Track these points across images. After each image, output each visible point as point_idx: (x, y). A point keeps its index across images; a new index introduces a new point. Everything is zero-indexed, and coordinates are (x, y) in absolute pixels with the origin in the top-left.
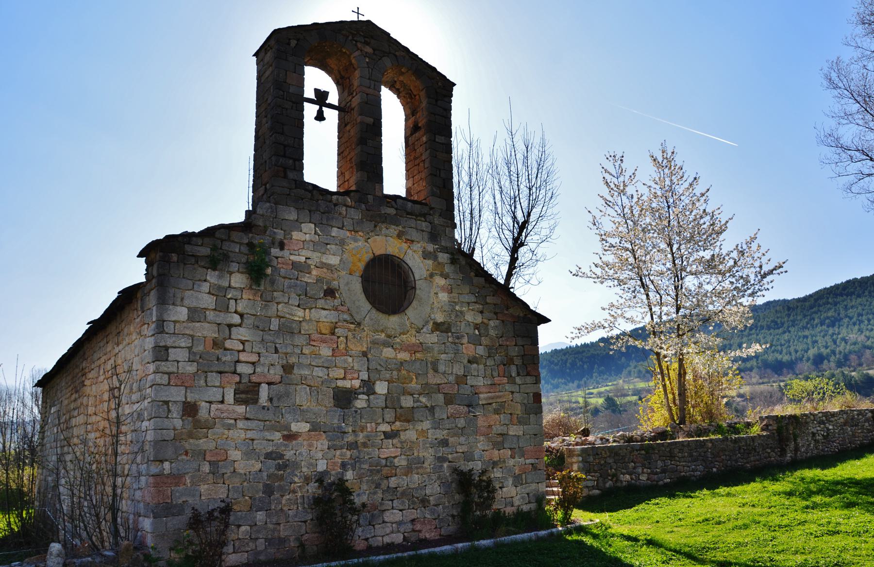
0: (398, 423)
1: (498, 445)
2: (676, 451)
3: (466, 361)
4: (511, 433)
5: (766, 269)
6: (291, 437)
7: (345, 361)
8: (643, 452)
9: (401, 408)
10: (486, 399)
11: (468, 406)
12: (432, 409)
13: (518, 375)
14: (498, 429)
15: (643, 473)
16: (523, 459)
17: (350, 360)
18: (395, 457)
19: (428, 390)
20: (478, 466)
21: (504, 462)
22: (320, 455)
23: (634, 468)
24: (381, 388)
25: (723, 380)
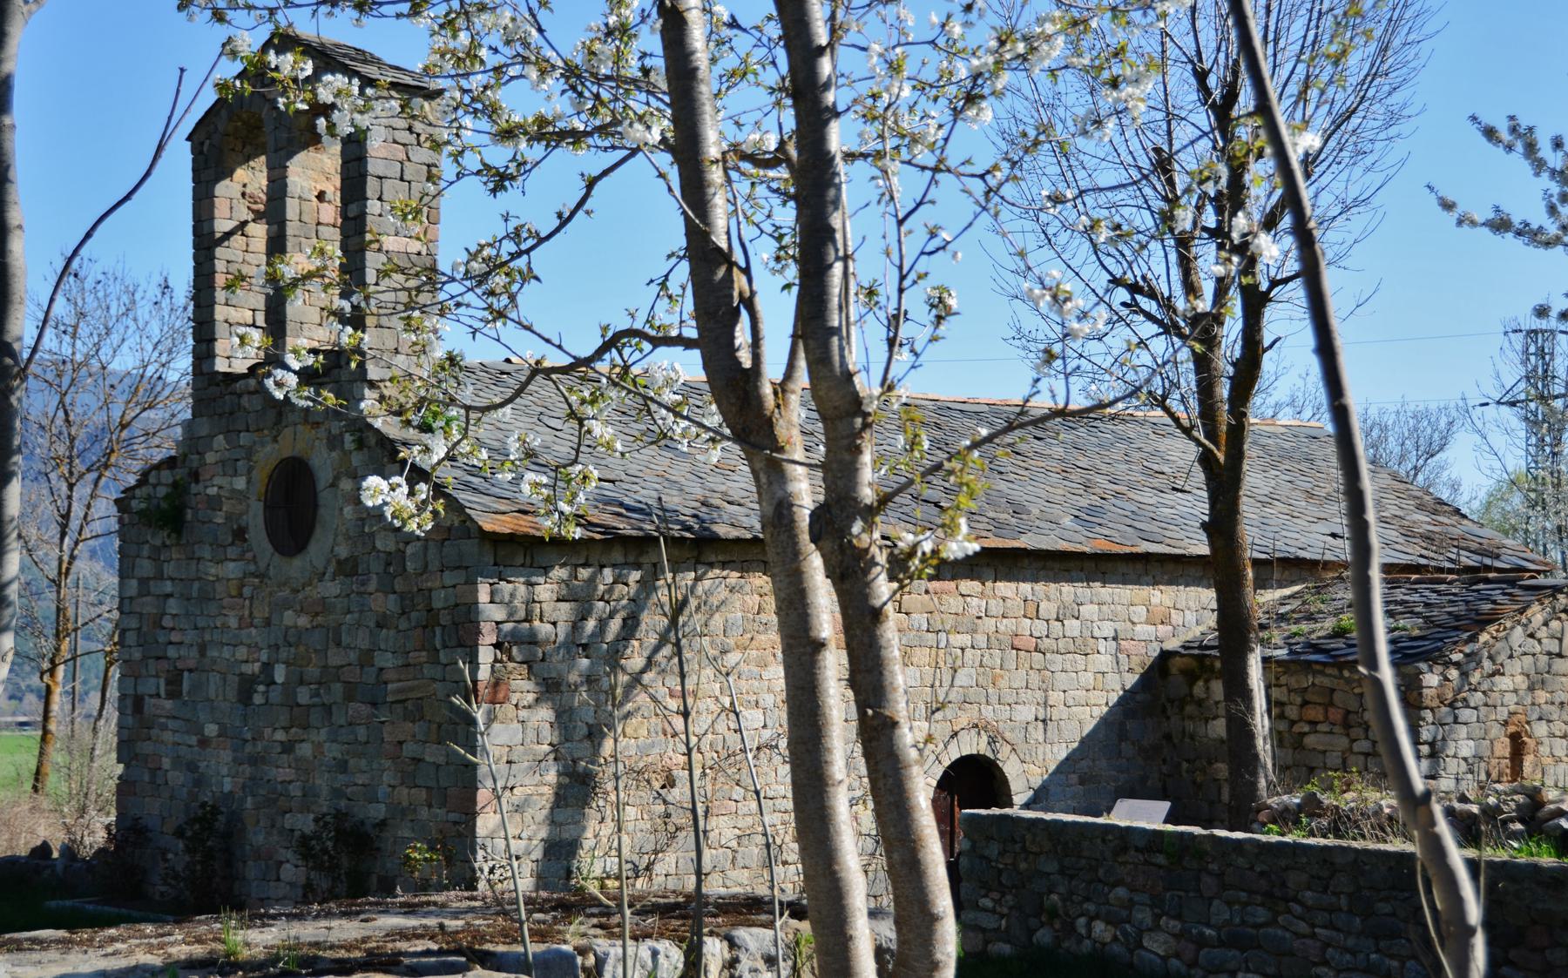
0: (293, 730)
1: (408, 780)
2: (1294, 879)
3: (372, 624)
4: (428, 759)
5: (901, 216)
6: (204, 742)
7: (249, 636)
8: (1161, 859)
9: (298, 705)
10: (400, 691)
11: (374, 704)
12: (328, 709)
13: (445, 647)
14: (410, 749)
15: (1156, 928)
16: (443, 811)
17: (253, 631)
18: (290, 782)
19: (329, 675)
20: (378, 811)
21: (415, 810)
22: (225, 771)
23: (1131, 904)
24: (280, 674)
25: (981, 640)
